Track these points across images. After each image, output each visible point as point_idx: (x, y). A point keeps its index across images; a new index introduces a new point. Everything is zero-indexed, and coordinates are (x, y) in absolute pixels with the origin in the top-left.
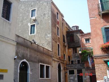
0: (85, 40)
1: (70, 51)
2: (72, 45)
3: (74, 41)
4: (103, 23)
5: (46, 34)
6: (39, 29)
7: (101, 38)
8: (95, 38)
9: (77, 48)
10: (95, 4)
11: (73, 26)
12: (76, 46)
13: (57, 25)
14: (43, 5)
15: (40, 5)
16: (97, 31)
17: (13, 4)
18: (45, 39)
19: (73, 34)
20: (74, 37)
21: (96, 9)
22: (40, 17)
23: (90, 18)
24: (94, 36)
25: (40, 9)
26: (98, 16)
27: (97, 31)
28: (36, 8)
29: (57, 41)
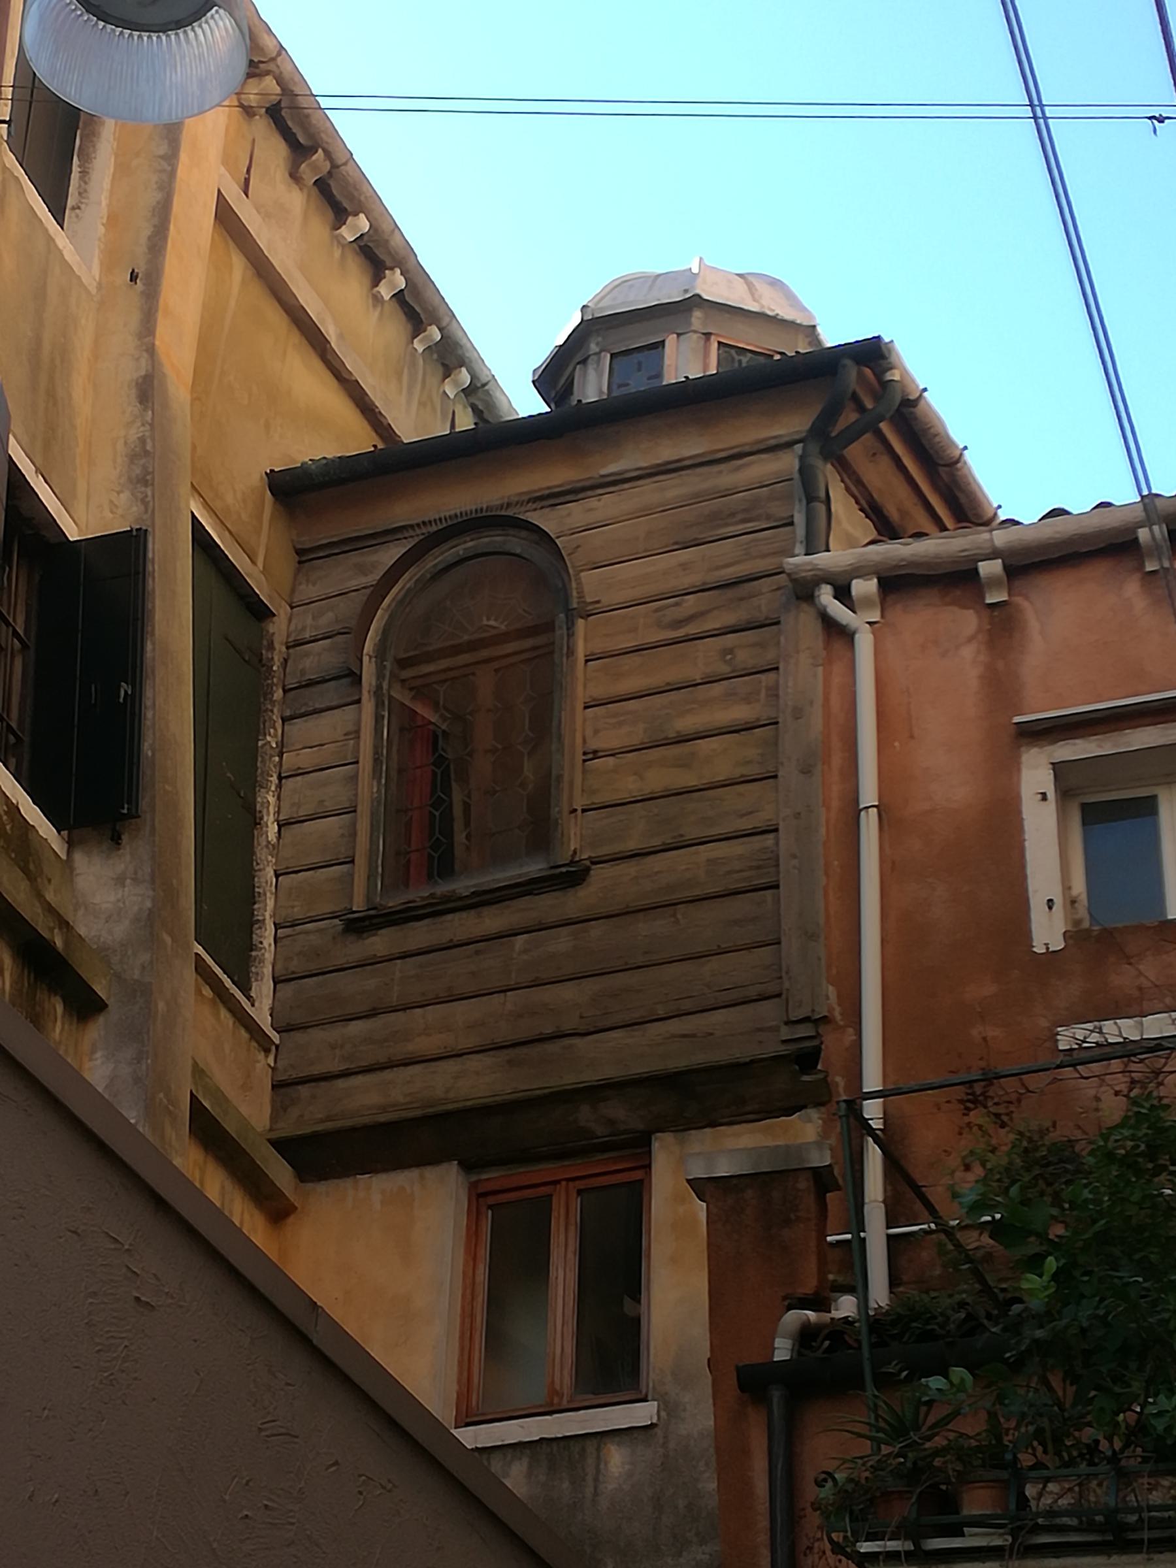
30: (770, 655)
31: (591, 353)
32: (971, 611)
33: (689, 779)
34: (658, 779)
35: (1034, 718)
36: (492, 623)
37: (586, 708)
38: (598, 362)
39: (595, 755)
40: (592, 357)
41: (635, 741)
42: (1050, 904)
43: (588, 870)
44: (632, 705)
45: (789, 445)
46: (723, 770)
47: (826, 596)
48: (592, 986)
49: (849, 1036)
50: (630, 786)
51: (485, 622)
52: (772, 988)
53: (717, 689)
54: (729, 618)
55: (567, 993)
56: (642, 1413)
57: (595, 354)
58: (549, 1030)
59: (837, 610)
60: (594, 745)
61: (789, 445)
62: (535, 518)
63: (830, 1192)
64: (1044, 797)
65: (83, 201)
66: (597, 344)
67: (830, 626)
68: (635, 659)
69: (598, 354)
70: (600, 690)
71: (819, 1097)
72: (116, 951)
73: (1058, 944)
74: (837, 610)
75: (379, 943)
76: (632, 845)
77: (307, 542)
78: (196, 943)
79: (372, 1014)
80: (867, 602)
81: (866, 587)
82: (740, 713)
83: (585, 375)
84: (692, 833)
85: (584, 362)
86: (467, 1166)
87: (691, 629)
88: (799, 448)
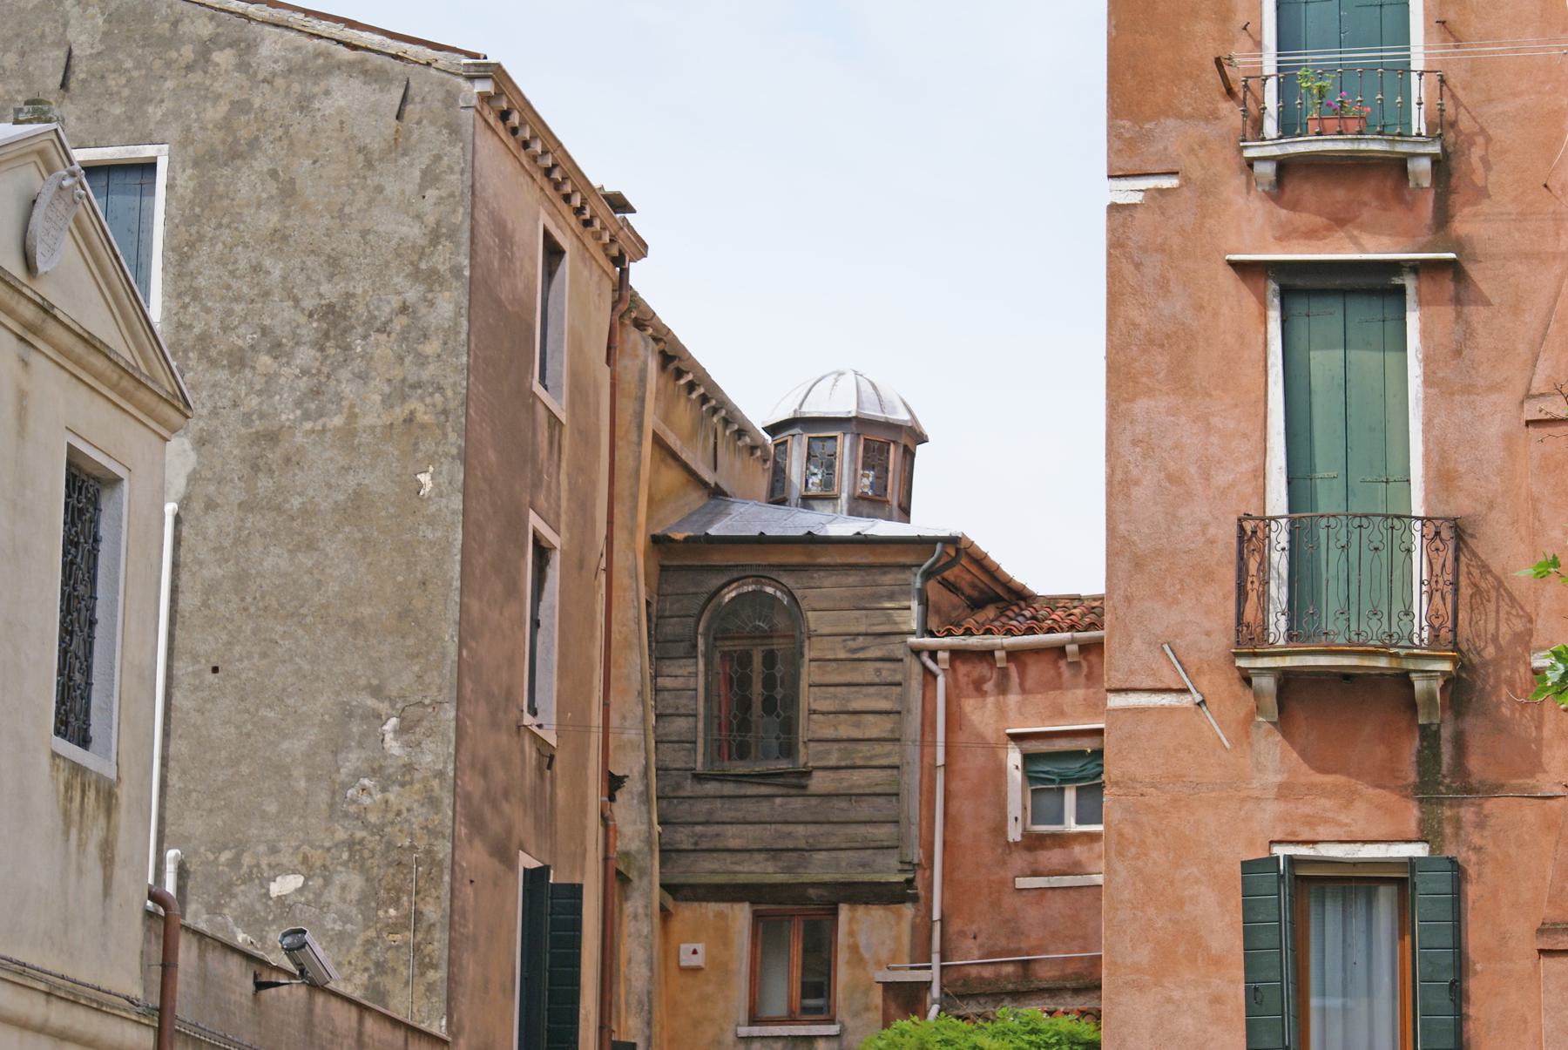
0: (1014, 758)
1: (691, 954)
2: (734, 837)
3: (806, 756)
4: (1285, 791)
5: (348, 713)
6: (212, 588)
7: (1217, 1000)
8: (1141, 988)
9: (844, 912)
10: (1206, 477)
11: (813, 409)
12: (821, 870)
13: (534, 520)
14: (303, 104)
15: (241, 107)
16: (1180, 902)
17: (126, 483)
18: (323, 797)
19: (795, 609)
20: (809, 673)
21: (1209, 576)
22: (239, 361)
23: (1278, 55)
24: (1144, 955)
25: (248, 182)
26: (1219, 685)
27: (1180, 902)
28: (161, 154)
29: (523, 825)
30: (898, 678)
33: (857, 734)
34: (845, 731)
35: (1274, 15)
36: (761, 624)
37: (810, 686)
39: (815, 712)
41: (832, 708)
42: (1016, 819)
43: (811, 772)
44: (832, 689)
46: (874, 733)
47: (925, 658)
48: (812, 829)
49: (927, 873)
50: (829, 733)
51: (757, 623)
52: (896, 844)
53: (872, 690)
54: (877, 653)
55: (800, 829)
56: (833, 1030)
58: (791, 846)
59: (930, 664)
60: (814, 706)
63: (685, 942)
64: (1017, 767)
67: (926, 670)
68: (834, 665)
70: (816, 679)
71: (915, 899)
73: (1018, 839)
74: (930, 664)
75: (711, 787)
76: (832, 763)
77: (666, 563)
78: (564, 421)
79: (706, 823)
80: (944, 661)
81: (943, 656)
82: (884, 705)
84: (860, 763)
86: (752, 903)
87: (861, 655)
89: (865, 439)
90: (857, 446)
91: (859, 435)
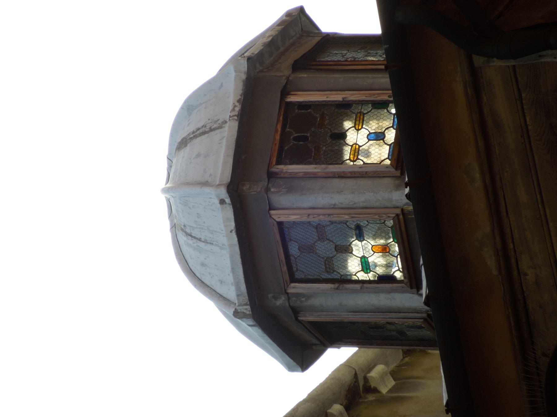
31: (287, 304)
32: (349, 261)
38: (297, 295)
40: (291, 304)
45: (474, 71)
57: (289, 299)
61: (474, 71)
62: (207, 229)
65: (381, 218)
66: (276, 298)
69: (289, 296)
72: (193, 208)
83: (312, 309)
85: (296, 311)
88: (478, 60)
89: (278, 163)
90: (294, 177)
91: (271, 176)
